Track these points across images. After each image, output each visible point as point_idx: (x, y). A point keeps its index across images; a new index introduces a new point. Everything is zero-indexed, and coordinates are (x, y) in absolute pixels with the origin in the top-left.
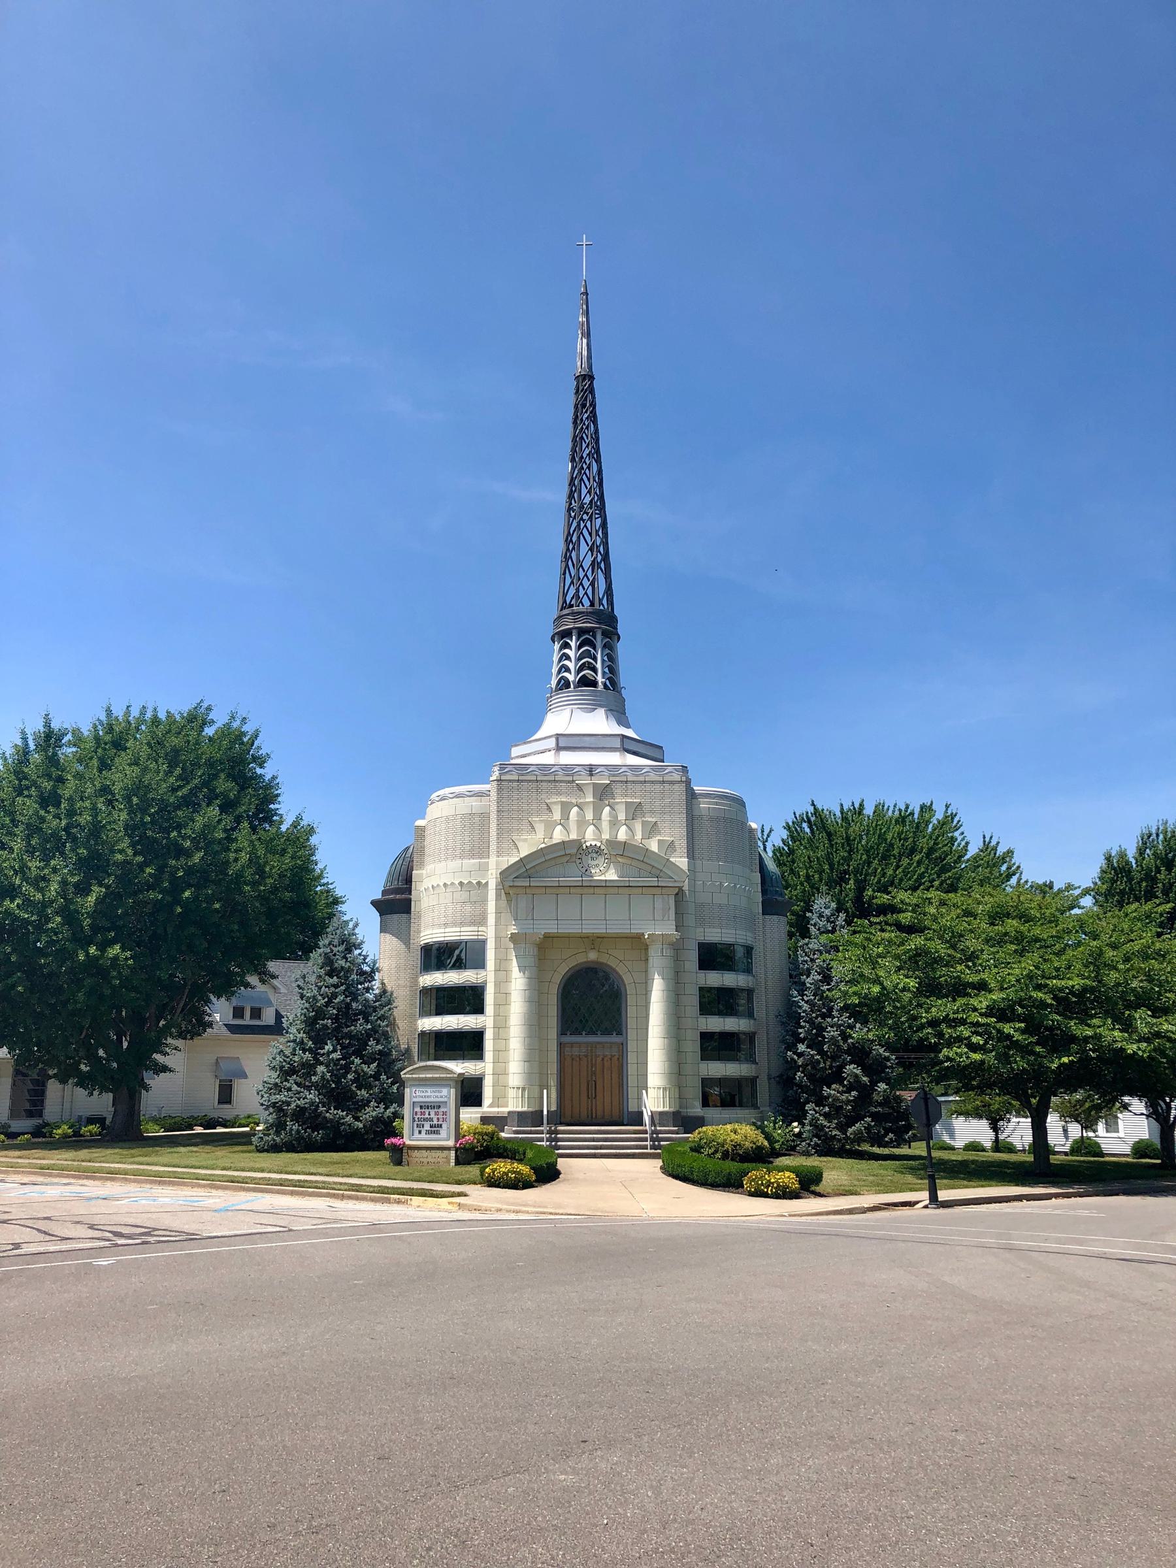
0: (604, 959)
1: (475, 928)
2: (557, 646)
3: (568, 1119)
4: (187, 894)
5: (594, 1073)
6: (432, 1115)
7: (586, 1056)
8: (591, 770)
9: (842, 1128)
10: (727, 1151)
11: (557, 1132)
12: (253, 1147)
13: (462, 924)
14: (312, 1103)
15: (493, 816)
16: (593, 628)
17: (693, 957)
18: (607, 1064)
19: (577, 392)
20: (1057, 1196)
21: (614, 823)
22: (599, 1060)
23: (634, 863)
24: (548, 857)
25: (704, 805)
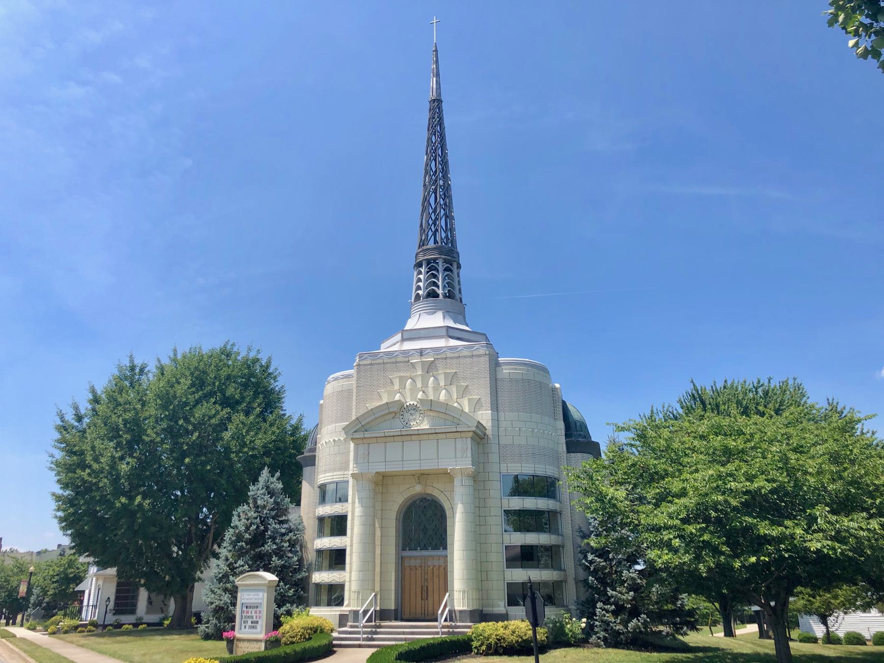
0: (429, 491)
2: (415, 273)
3: (406, 616)
4: (187, 460)
5: (426, 580)
7: (421, 566)
8: (421, 352)
9: (625, 623)
11: (380, 627)
13: (334, 470)
14: (225, 603)
15: (355, 390)
18: (436, 573)
21: (437, 389)
22: (430, 569)
23: (441, 415)
25: (506, 371)
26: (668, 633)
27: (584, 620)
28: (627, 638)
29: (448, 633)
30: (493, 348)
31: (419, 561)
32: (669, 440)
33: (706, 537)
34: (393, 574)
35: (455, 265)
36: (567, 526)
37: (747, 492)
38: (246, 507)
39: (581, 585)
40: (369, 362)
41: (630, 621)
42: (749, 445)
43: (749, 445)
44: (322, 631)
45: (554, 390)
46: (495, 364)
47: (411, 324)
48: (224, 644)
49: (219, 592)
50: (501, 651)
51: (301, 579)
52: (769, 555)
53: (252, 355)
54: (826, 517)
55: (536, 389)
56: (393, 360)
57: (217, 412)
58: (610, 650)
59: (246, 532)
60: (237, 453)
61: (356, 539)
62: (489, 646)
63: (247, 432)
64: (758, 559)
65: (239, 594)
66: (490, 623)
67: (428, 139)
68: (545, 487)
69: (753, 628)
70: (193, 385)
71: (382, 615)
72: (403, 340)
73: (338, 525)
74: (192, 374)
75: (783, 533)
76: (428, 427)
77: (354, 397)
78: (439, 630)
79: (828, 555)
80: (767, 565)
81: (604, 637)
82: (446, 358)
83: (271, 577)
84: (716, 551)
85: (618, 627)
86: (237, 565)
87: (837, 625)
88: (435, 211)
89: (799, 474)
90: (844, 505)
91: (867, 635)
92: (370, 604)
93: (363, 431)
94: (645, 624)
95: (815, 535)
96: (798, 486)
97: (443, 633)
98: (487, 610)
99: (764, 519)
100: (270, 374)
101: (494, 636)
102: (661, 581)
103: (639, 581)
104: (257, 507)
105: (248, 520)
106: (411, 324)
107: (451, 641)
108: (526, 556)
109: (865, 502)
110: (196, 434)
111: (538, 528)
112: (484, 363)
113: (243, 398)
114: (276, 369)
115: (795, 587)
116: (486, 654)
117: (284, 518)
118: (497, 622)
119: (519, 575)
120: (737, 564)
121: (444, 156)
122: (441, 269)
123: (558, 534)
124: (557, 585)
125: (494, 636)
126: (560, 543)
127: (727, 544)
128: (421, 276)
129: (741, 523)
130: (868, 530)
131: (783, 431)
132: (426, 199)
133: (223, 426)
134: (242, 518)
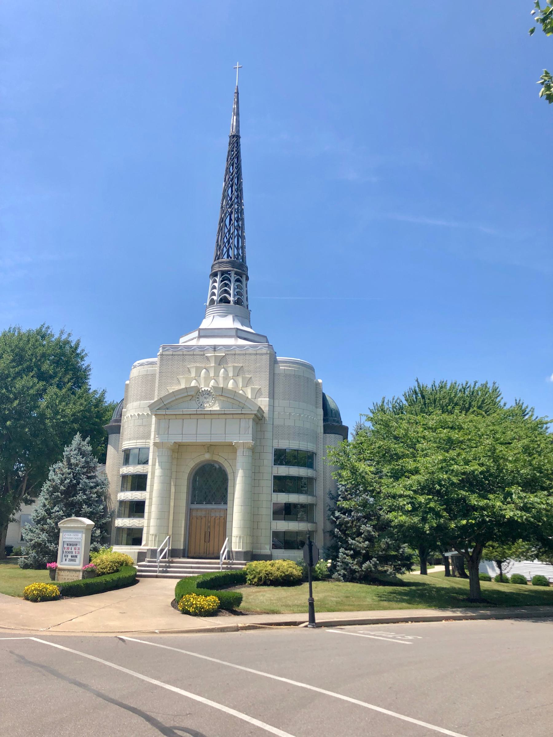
0: (216, 458)
1: (144, 441)
2: (211, 281)
4: (8, 423)
5: (209, 527)
6: (73, 550)
7: (205, 517)
8: (215, 348)
9: (360, 564)
10: (261, 577)
11: (173, 562)
12: (18, 566)
13: (138, 438)
14: (43, 541)
15: (157, 376)
16: (233, 273)
17: (269, 457)
18: (217, 522)
19: (229, 145)
20: (447, 619)
21: (226, 378)
22: (213, 519)
23: (229, 400)
24: (177, 397)
25: (282, 367)
26: (391, 573)
27: (330, 561)
28: (360, 576)
29: (227, 568)
30: (273, 349)
31: (204, 513)
32: (407, 430)
33: (432, 505)
34: (183, 522)
35: (244, 277)
36: (320, 489)
37: (464, 473)
38: (61, 464)
39: (328, 535)
40: (171, 353)
41: (364, 562)
42: (466, 437)
43: (466, 437)
44: (127, 564)
45: (317, 384)
46: (274, 362)
47: (206, 324)
48: (47, 572)
49: (37, 531)
50: (269, 583)
51: (105, 524)
52: (475, 519)
53: (64, 337)
54: (519, 493)
55: (303, 381)
56: (191, 353)
57: (34, 385)
58: (348, 584)
59: (61, 484)
60: (51, 419)
61: (155, 494)
62: (260, 579)
63: (60, 402)
64: (468, 521)
65: (61, 534)
66: (261, 562)
67: (227, 168)
68: (306, 459)
69: (441, 568)
70: (13, 361)
71: (174, 553)
72: (200, 337)
73: (139, 482)
74: (12, 351)
75: (487, 504)
76: (218, 409)
77: (157, 381)
78: (220, 566)
79: (517, 521)
80: (472, 525)
81: (344, 574)
82: (235, 354)
83: (88, 522)
84: (438, 515)
85: (354, 567)
86: (54, 511)
87: (508, 569)
88: (229, 231)
89: (501, 461)
90: (531, 485)
91: (528, 577)
92: (165, 545)
93: (166, 409)
94: (375, 565)
95: (509, 505)
96: (499, 469)
97: (223, 568)
98: (257, 551)
99: (473, 492)
100: (78, 354)
101: (264, 572)
102: (391, 536)
103: (373, 533)
104: (71, 465)
105: (63, 474)
106: (206, 324)
107: (232, 574)
108: (287, 511)
109: (545, 482)
110: (17, 402)
111: (298, 491)
112: (265, 360)
113: (56, 373)
114: (83, 350)
115: (488, 541)
116: (258, 584)
117: (92, 474)
118: (266, 561)
119: (283, 526)
120: (453, 526)
121: (239, 184)
122: (233, 280)
123: (313, 495)
124: (311, 534)
125: (264, 572)
126: (314, 503)
127: (445, 510)
128: (216, 285)
129: (458, 495)
130: (547, 503)
131: (491, 428)
132: (222, 220)
133: (40, 394)
134: (57, 473)
